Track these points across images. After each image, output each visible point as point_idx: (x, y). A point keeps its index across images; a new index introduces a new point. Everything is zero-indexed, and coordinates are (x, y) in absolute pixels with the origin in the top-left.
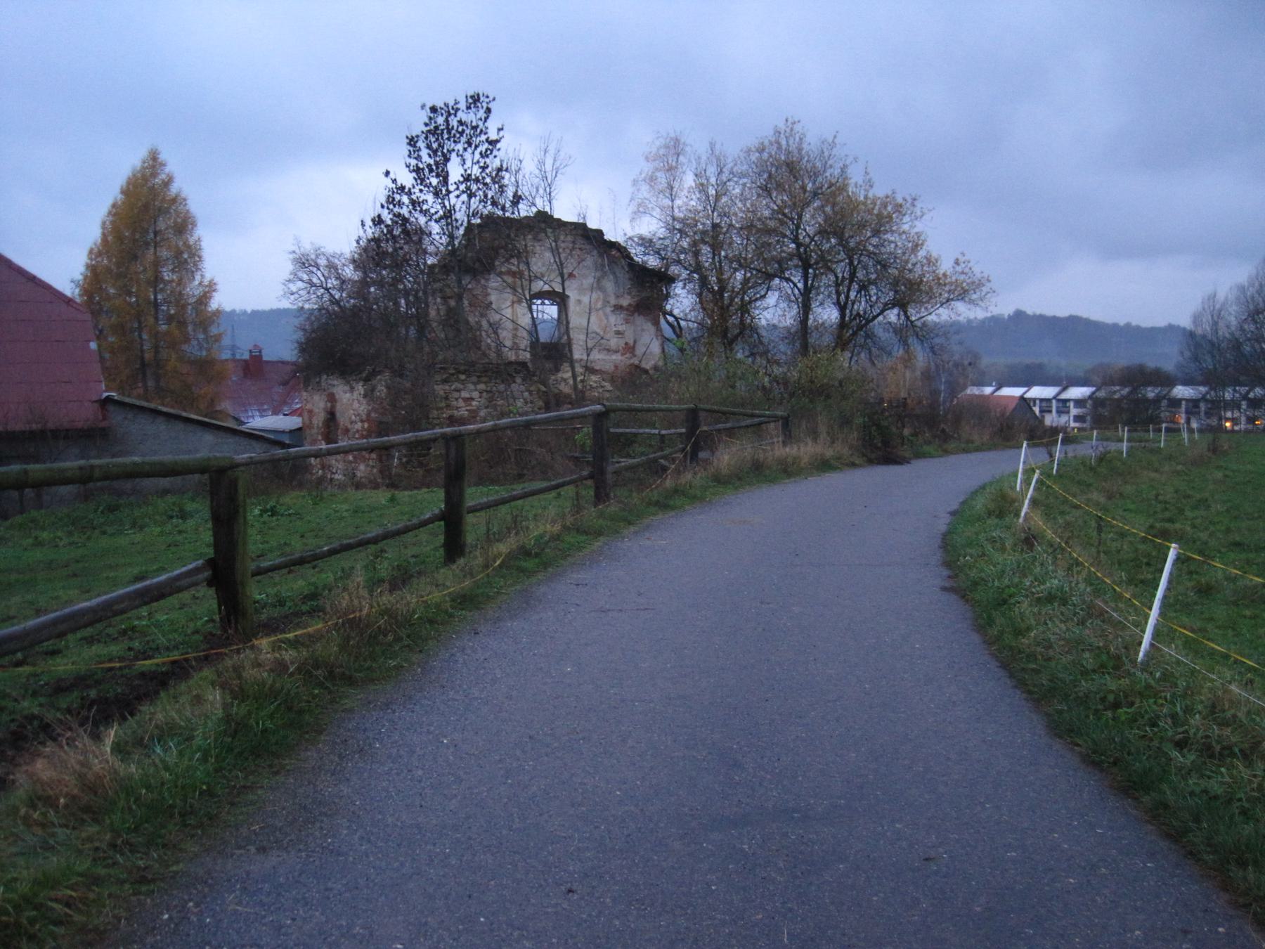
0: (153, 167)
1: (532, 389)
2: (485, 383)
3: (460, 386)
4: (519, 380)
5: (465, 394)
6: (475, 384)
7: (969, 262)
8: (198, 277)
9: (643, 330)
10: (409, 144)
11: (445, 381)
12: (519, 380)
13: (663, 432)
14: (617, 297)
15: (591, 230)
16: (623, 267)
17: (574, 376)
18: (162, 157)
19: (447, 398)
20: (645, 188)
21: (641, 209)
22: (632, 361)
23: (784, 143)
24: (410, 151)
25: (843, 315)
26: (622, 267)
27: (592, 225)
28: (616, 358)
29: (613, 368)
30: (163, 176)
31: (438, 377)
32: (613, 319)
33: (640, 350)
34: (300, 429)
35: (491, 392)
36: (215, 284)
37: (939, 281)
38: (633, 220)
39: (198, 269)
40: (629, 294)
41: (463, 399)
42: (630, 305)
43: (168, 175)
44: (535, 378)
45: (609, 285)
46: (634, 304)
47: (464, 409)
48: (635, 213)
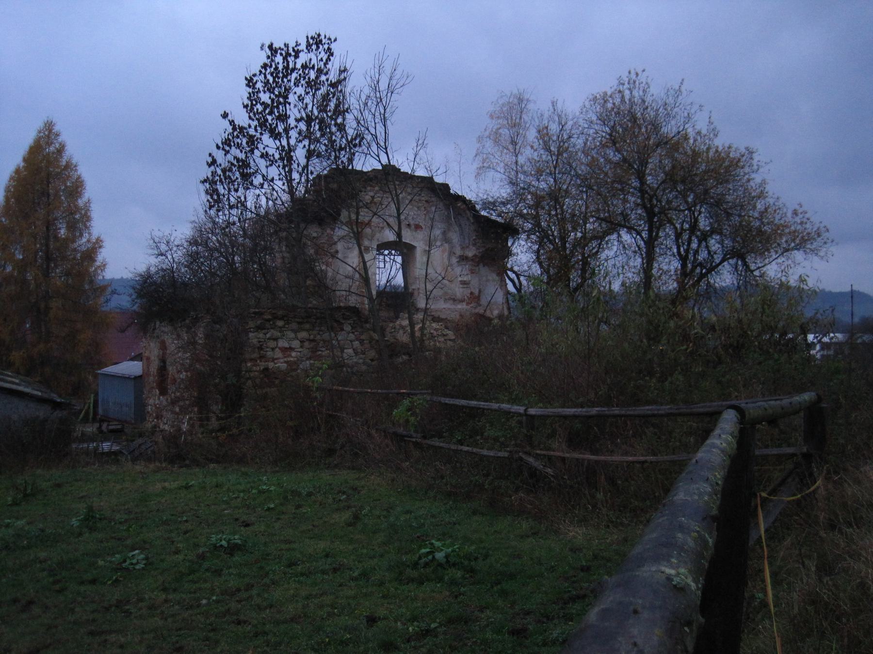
0: (48, 137)
1: (363, 337)
2: (307, 330)
3: (278, 334)
4: (348, 328)
5: (283, 343)
6: (295, 332)
7: (806, 213)
8: (86, 235)
9: (488, 281)
10: (248, 85)
11: (259, 328)
12: (348, 328)
13: (532, 411)
14: (463, 248)
15: (438, 184)
16: (468, 219)
17: (412, 325)
18: (56, 129)
19: (260, 348)
20: (489, 144)
21: (485, 164)
22: (477, 311)
23: (627, 93)
24: (249, 93)
25: (684, 266)
26: (468, 219)
27: (438, 179)
29: (458, 317)
30: (57, 146)
31: (251, 324)
32: (458, 270)
33: (484, 302)
34: (141, 377)
35: (313, 340)
36: (101, 241)
37: (779, 230)
38: (478, 175)
39: (87, 227)
40: (474, 245)
41: (280, 348)
42: (475, 256)
43: (60, 144)
44: (368, 326)
45: (455, 237)
46: (480, 255)
47: (282, 360)
48: (480, 168)
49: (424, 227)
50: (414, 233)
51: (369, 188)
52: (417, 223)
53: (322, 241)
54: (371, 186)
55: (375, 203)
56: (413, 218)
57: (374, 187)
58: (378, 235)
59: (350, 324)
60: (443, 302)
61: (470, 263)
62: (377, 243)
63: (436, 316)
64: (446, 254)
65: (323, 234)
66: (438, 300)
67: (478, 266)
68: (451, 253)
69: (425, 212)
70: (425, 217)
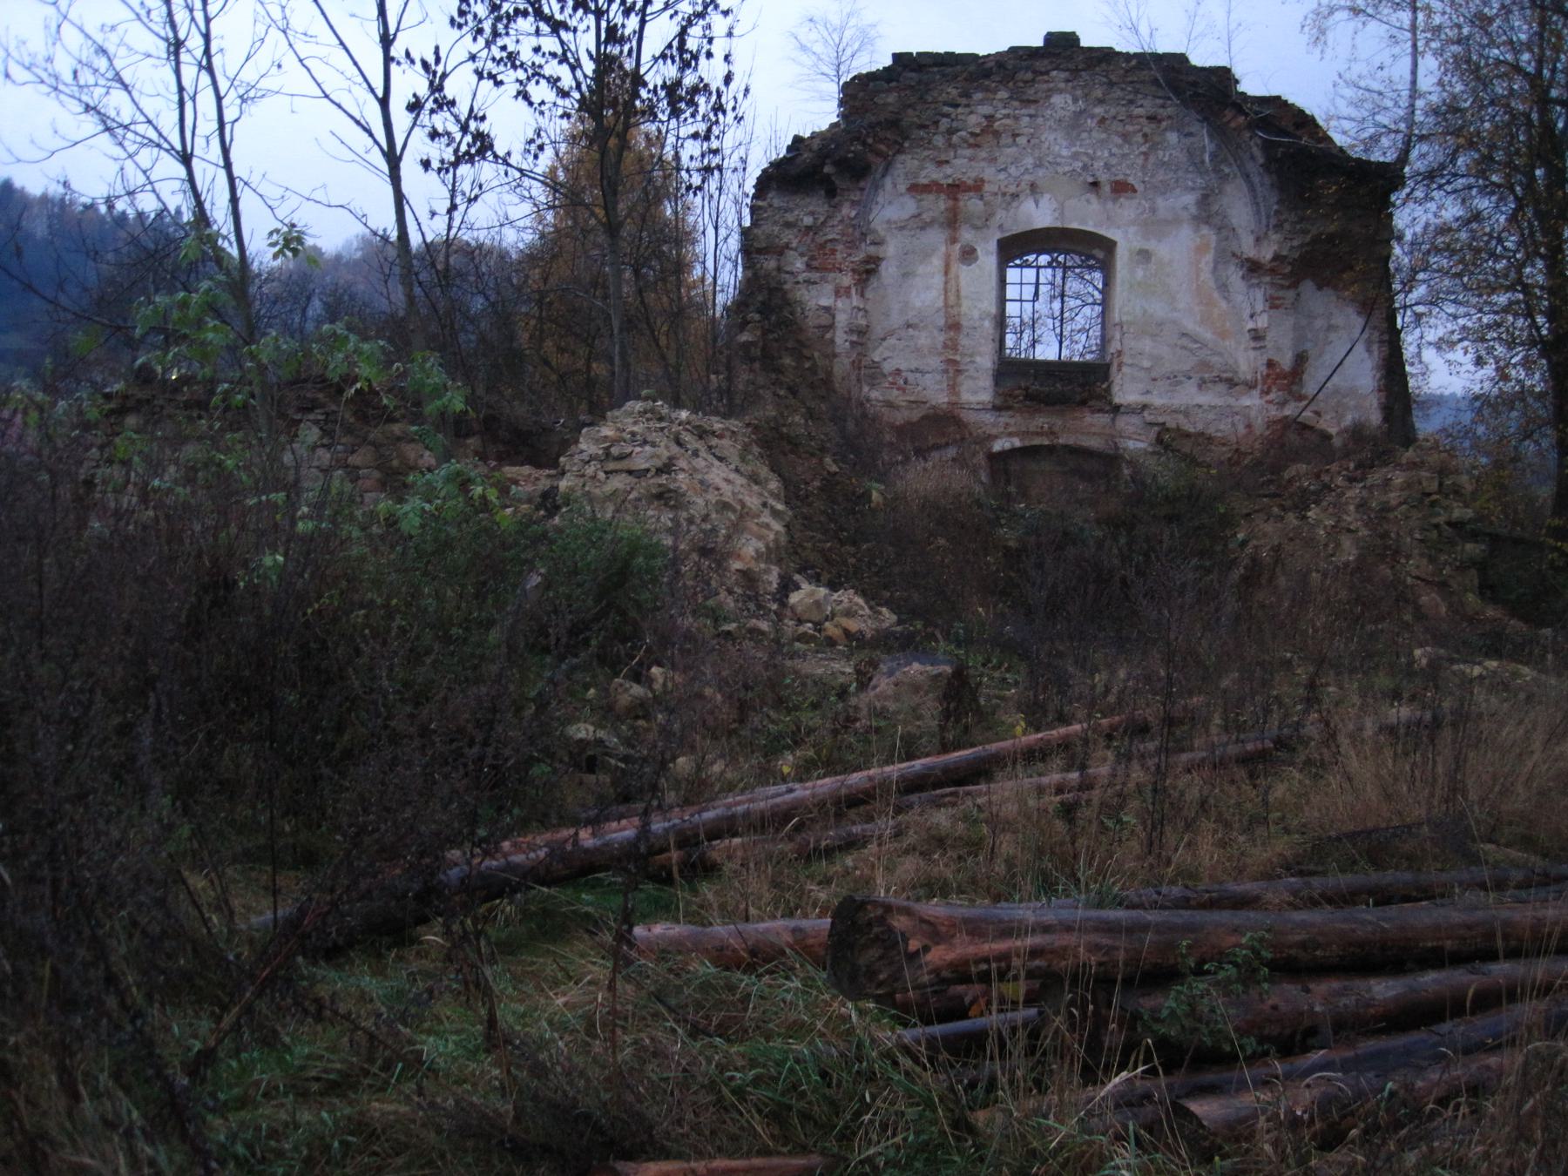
1: (354, 460)
28: (1252, 401)
29: (1242, 430)
40: (1278, 227)
49: (1139, 187)
50: (1110, 205)
51: (978, 96)
52: (1120, 177)
53: (830, 237)
54: (987, 90)
55: (997, 134)
56: (1107, 166)
57: (995, 91)
58: (1000, 215)
59: (316, 422)
60: (1194, 390)
61: (1267, 279)
62: (999, 235)
63: (1171, 424)
64: (1209, 257)
65: (829, 217)
66: (1180, 383)
67: (1295, 285)
68: (1225, 255)
69: (1143, 149)
70: (1146, 160)
